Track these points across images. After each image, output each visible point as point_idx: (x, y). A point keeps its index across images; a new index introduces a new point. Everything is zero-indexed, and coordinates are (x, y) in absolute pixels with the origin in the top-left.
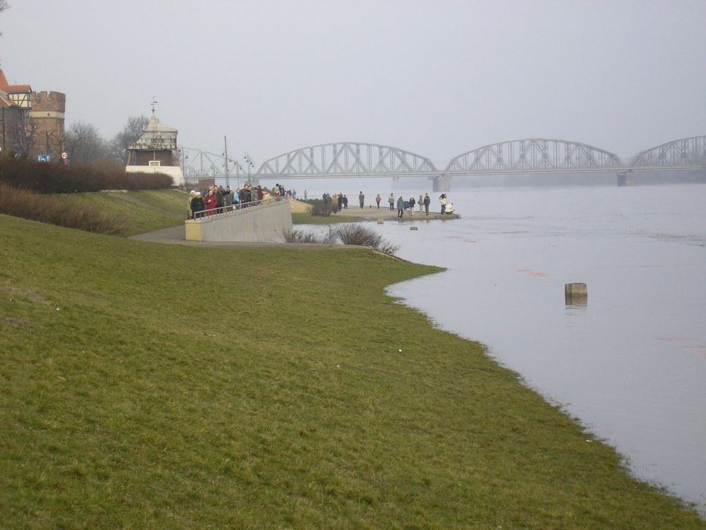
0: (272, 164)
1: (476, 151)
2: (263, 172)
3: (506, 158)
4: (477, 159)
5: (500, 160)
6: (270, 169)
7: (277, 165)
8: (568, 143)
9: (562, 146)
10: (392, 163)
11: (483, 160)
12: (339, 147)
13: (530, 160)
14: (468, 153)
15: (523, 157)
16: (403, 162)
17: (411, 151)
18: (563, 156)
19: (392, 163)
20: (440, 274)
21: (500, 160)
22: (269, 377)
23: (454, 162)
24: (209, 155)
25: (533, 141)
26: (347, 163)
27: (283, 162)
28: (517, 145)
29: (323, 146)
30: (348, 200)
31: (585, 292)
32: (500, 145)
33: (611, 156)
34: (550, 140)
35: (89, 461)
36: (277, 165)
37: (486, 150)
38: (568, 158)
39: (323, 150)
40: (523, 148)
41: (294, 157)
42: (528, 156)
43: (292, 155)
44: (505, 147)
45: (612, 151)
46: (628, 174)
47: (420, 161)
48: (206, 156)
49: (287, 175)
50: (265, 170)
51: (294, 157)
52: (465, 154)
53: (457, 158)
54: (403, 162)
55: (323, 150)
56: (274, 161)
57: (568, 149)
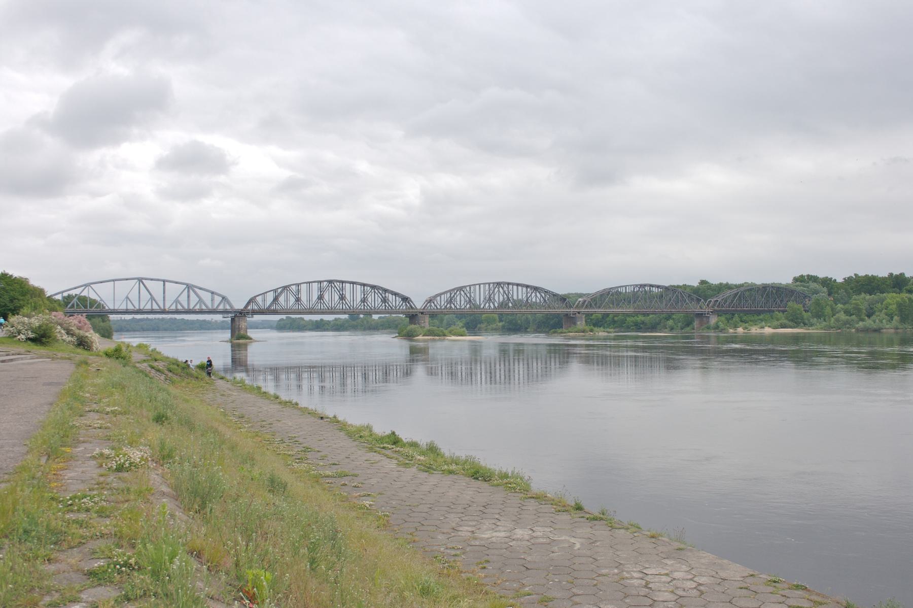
0: (259, 299)
1: (275, 291)
3: (304, 298)
4: (276, 299)
5: (342, 298)
6: (205, 305)
9: (487, 286)
10: (287, 300)
11: (282, 299)
13: (327, 300)
14: (266, 293)
15: (321, 297)
16: (384, 300)
17: (219, 292)
18: (359, 298)
19: (287, 300)
21: (298, 300)
23: (430, 301)
24: (196, 290)
25: (330, 282)
27: (270, 297)
28: (315, 286)
29: (480, 285)
31: (392, 381)
32: (298, 285)
33: (405, 299)
35: (121, 445)
36: (264, 300)
37: (284, 289)
38: (364, 300)
39: (480, 286)
40: (321, 290)
41: (281, 292)
42: (326, 297)
44: (304, 287)
46: (577, 314)
47: (218, 299)
48: (194, 291)
50: (225, 306)
51: (281, 292)
52: (264, 294)
53: (255, 297)
54: (384, 300)
55: (480, 286)
56: (261, 297)
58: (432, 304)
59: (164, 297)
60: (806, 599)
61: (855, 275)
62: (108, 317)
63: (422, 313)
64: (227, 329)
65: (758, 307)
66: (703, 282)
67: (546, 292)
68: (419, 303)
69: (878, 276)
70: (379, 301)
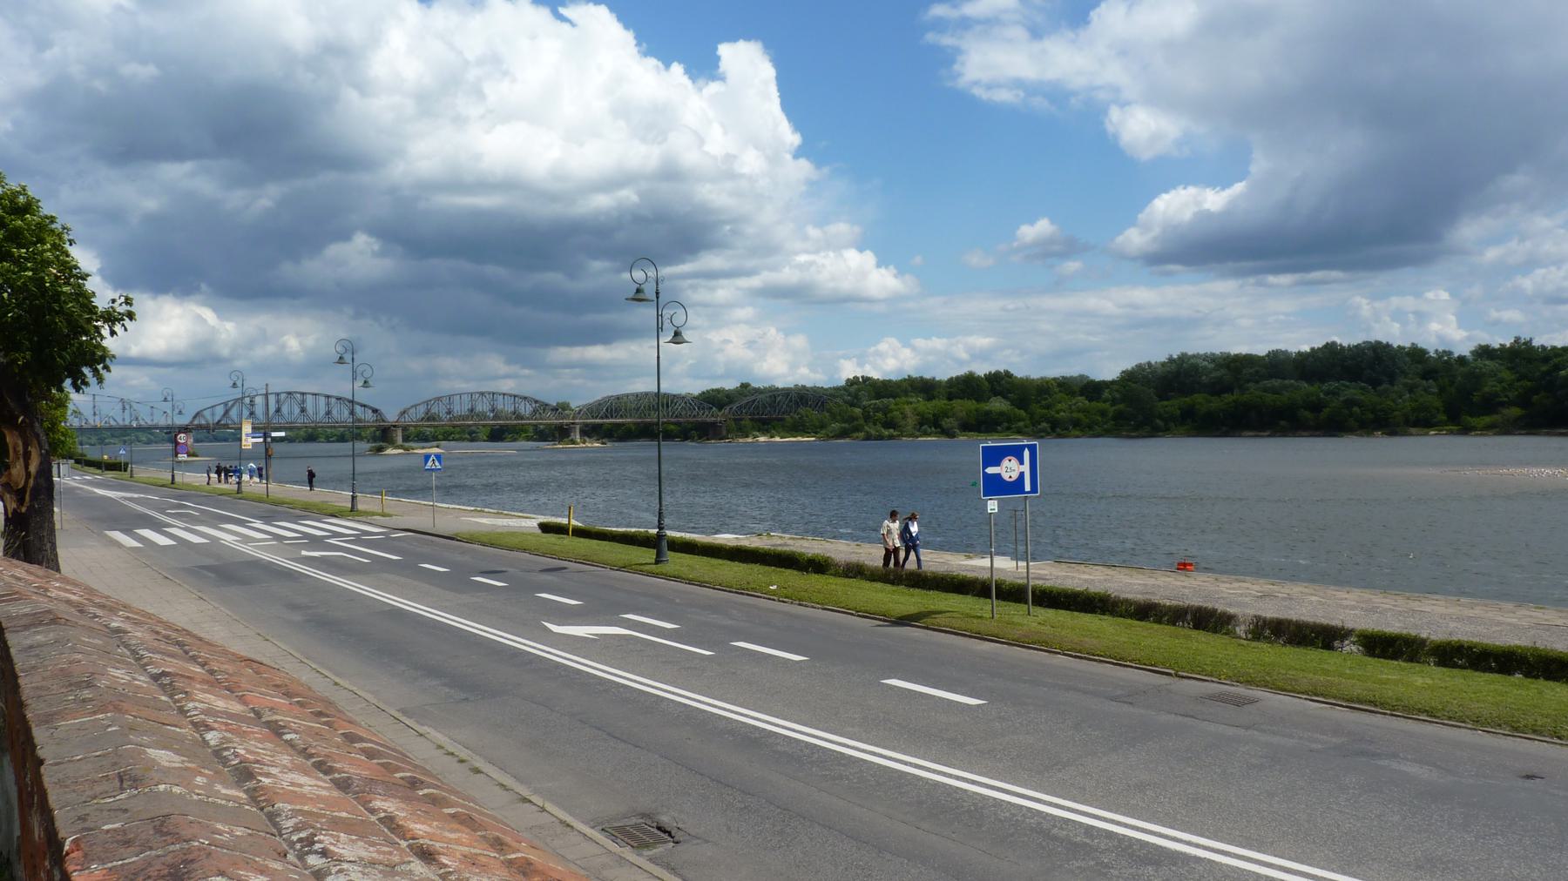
0: (207, 413)
1: (226, 404)
2: (196, 422)
4: (226, 413)
5: (303, 410)
7: (213, 414)
8: (328, 397)
9: (322, 400)
12: (283, 396)
16: (352, 413)
20: (566, 26)
22: (1290, 599)
23: (197, 415)
25: (290, 393)
26: (291, 413)
27: (220, 411)
30: (1379, 340)
33: (375, 411)
34: (309, 393)
36: (213, 414)
38: (328, 413)
41: (233, 406)
42: (285, 409)
43: (230, 404)
45: (377, 407)
49: (225, 425)
51: (233, 406)
52: (212, 407)
54: (352, 413)
57: (328, 404)
58: (406, 416)
59: (658, 357)
60: (1350, 647)
61: (909, 376)
62: (145, 753)
63: (395, 426)
64: (996, 569)
65: (762, 414)
66: (1123, 372)
67: (536, 402)
68: (391, 416)
69: (934, 378)
70: (346, 413)
